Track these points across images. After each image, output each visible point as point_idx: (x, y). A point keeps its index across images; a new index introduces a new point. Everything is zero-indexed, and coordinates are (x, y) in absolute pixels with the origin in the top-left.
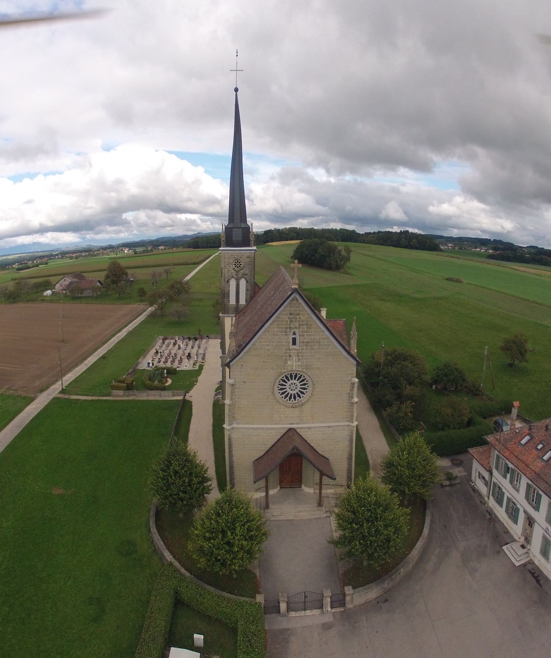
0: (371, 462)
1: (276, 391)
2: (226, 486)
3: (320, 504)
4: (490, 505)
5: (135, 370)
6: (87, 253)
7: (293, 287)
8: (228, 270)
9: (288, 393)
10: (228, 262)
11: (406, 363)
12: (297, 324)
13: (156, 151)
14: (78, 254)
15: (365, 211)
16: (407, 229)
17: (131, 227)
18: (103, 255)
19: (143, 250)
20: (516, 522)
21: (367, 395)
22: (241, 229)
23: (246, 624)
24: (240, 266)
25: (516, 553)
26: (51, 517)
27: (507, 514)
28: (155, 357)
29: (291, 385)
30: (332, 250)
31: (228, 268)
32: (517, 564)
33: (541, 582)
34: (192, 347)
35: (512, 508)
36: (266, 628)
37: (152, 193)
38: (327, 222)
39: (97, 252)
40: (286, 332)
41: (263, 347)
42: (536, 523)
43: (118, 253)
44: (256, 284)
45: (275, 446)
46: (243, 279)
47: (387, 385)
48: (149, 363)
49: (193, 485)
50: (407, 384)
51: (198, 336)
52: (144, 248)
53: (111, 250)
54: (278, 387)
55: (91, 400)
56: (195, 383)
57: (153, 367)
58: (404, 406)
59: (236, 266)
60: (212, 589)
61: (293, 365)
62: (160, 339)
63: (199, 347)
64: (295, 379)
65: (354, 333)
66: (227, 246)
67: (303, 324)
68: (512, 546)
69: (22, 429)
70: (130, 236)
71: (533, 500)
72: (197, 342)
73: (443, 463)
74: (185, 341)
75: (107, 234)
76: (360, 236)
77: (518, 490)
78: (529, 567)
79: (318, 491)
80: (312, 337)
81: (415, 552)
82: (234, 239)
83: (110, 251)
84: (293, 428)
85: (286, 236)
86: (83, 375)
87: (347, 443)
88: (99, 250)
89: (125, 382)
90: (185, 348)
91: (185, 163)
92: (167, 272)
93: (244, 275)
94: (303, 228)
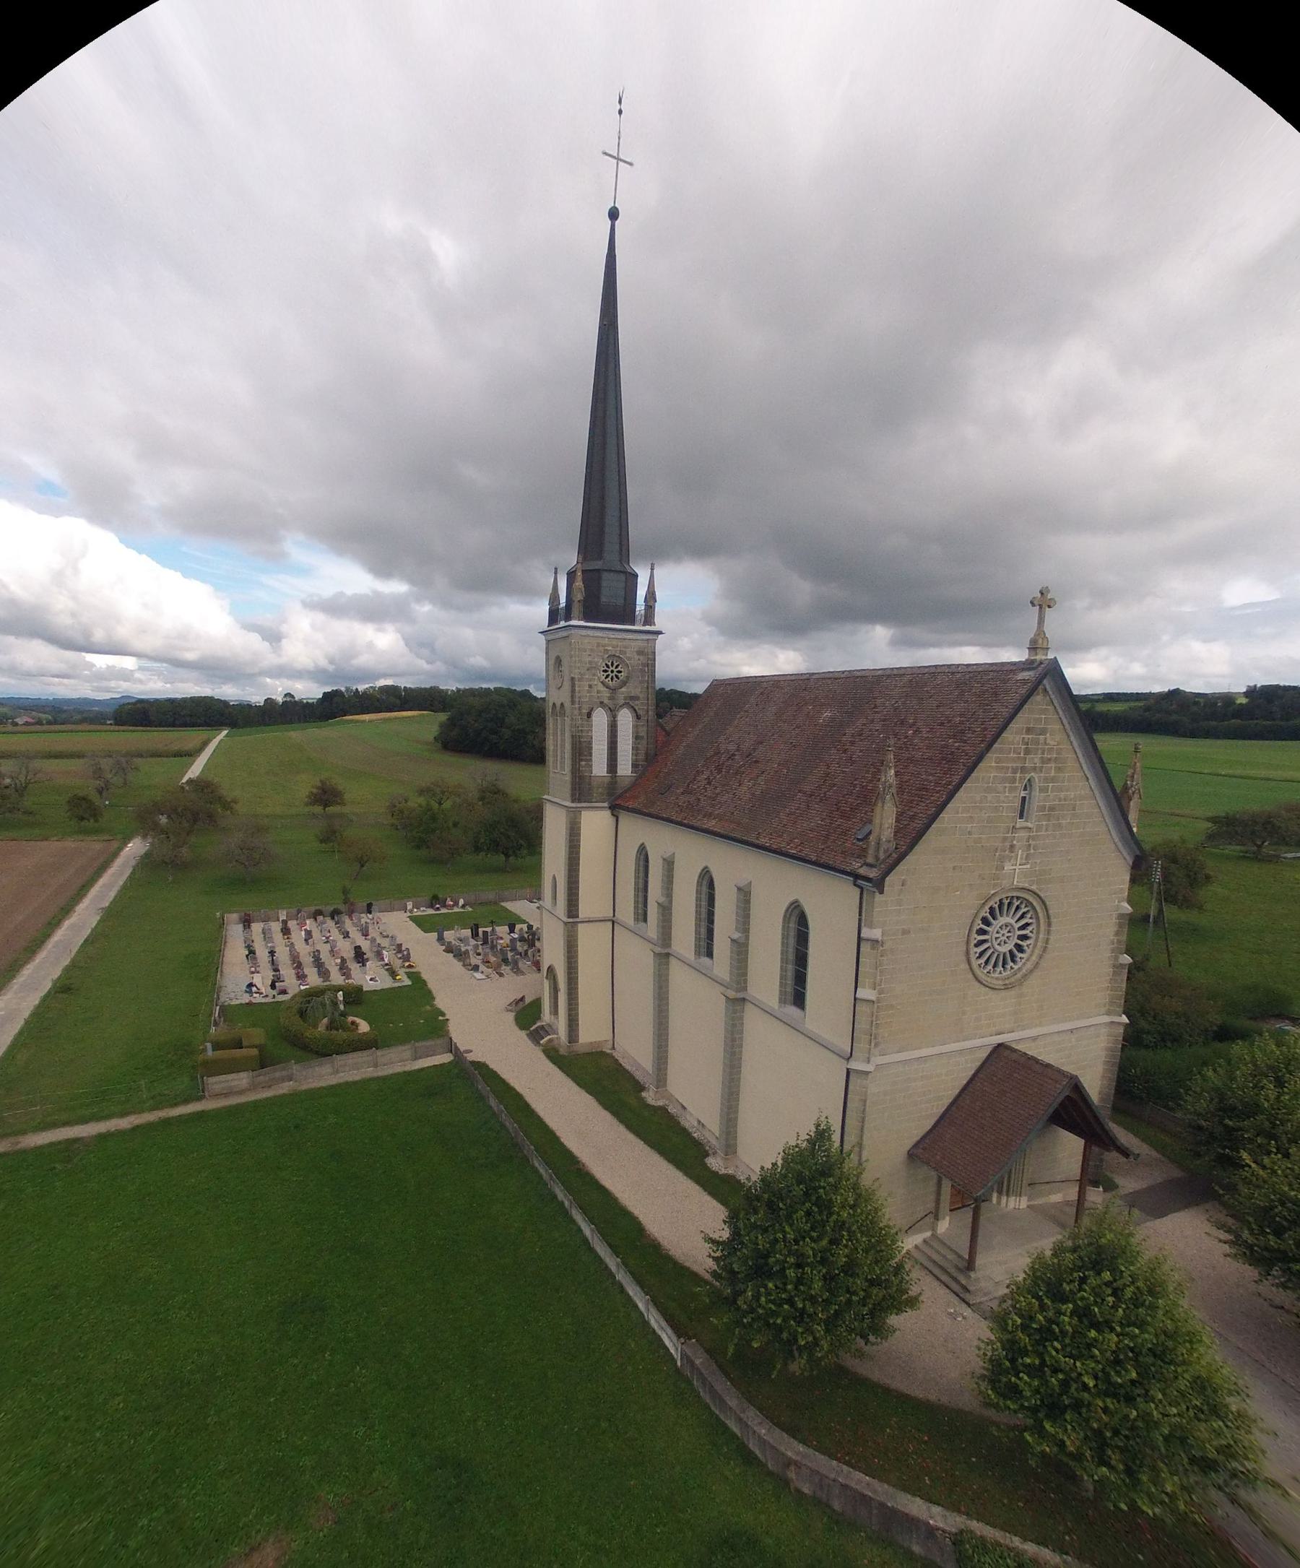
8: (590, 686)
24: (620, 675)
51: (342, 907)
61: (1016, 873)
66: (587, 619)
67: (1050, 759)
80: (1062, 795)
82: (604, 599)
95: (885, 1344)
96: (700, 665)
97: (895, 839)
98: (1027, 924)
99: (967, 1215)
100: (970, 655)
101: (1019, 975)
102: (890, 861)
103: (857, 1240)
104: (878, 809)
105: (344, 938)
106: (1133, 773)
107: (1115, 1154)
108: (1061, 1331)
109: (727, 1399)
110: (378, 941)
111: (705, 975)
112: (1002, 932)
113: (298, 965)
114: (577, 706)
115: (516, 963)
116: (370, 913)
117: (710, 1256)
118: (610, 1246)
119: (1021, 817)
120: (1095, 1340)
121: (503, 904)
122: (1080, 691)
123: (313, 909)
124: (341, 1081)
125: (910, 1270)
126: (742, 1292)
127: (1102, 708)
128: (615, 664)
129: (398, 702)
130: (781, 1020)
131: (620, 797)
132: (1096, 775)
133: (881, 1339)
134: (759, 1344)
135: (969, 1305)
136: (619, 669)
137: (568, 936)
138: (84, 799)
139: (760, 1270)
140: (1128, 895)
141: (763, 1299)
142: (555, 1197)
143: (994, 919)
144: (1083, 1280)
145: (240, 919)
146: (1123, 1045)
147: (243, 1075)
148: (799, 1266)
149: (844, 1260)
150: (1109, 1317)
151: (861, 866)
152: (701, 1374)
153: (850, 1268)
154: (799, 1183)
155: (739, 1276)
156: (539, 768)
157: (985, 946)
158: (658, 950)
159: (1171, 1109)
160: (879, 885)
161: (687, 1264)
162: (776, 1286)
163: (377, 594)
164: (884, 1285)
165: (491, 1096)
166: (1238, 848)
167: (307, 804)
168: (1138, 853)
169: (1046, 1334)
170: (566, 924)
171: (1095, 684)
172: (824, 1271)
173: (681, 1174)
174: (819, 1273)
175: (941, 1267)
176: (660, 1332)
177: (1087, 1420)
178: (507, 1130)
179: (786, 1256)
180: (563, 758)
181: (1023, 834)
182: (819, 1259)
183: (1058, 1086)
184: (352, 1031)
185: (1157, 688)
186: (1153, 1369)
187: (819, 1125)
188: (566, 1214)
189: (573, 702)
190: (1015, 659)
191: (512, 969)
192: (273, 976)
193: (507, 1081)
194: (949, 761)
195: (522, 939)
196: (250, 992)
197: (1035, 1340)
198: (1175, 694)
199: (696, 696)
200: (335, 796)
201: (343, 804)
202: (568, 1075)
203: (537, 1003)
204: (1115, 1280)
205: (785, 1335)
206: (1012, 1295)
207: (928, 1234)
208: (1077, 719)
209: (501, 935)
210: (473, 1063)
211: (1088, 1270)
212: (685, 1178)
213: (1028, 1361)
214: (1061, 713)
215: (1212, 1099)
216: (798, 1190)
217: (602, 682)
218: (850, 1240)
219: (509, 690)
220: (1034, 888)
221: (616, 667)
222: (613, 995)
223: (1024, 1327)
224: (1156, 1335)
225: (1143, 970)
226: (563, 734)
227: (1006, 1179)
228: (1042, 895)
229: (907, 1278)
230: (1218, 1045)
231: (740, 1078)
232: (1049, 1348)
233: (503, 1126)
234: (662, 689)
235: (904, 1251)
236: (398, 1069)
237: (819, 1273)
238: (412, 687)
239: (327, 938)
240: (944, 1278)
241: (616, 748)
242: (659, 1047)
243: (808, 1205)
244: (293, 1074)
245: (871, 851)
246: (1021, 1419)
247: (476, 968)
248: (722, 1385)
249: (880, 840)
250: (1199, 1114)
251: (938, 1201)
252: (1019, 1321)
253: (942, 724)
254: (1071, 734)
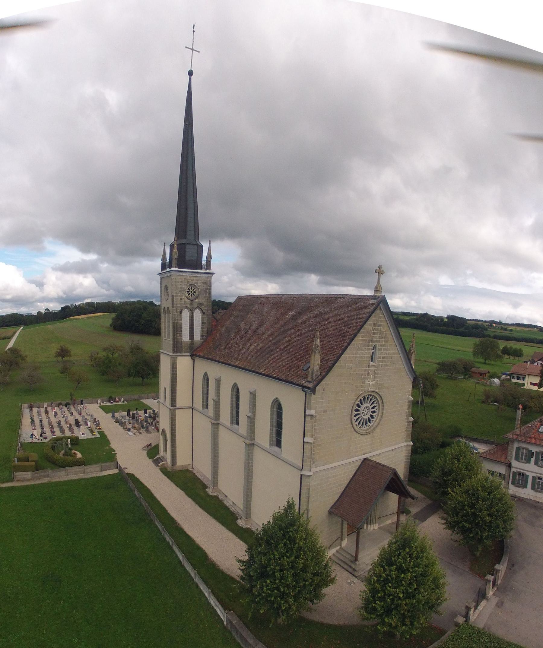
8: (181, 299)
10: (181, 288)
24: (195, 293)
51: (70, 402)
61: (370, 384)
67: (382, 337)
69: (287, 458)
80: (387, 352)
82: (187, 258)
95: (321, 603)
96: (232, 289)
97: (320, 370)
98: (375, 406)
99: (354, 536)
100: (351, 291)
101: (372, 428)
102: (318, 380)
103: (307, 555)
104: (313, 357)
105: (71, 415)
106: (413, 345)
107: (409, 499)
108: (391, 579)
109: (249, 640)
110: (86, 417)
111: (235, 433)
112: (365, 410)
113: (52, 427)
114: (175, 308)
115: (147, 428)
116: (82, 404)
117: (239, 569)
118: (192, 564)
119: (372, 361)
120: (403, 578)
121: (141, 400)
122: (393, 310)
123: (58, 402)
124: (69, 479)
125: (331, 566)
126: (255, 586)
127: (401, 317)
128: (193, 288)
129: (94, 309)
130: (271, 453)
131: (195, 350)
132: (400, 344)
133: (319, 601)
134: (263, 611)
135: (356, 577)
136: (194, 291)
137: (172, 415)
139: (263, 574)
140: (412, 393)
141: (265, 588)
142: (165, 539)
143: (362, 405)
144: (399, 554)
145: (28, 406)
146: (411, 454)
147: (29, 473)
148: (281, 570)
149: (302, 565)
150: (408, 567)
151: (306, 382)
152: (236, 628)
153: (304, 569)
154: (280, 530)
155: (254, 578)
156: (158, 337)
157: (358, 416)
158: (213, 421)
159: (428, 477)
160: (313, 390)
161: (228, 573)
162: (271, 582)
163: (84, 261)
164: (320, 575)
165: (136, 490)
166: (446, 374)
167: (55, 357)
168: (415, 376)
169: (386, 581)
170: (170, 409)
171: (398, 308)
172: (293, 572)
173: (225, 528)
174: (291, 573)
175: (344, 562)
176: (216, 608)
177: (400, 611)
178: (143, 506)
179: (275, 566)
180: (169, 333)
181: (373, 368)
182: (290, 566)
183: (388, 474)
184: (74, 457)
185: (420, 312)
186: (421, 581)
187: (289, 502)
188: (170, 548)
189: (173, 307)
190: (369, 294)
191: (145, 431)
192: (41, 431)
193: (143, 483)
194: (343, 336)
195: (150, 417)
196: (32, 438)
197: (382, 585)
198: (426, 314)
199: (230, 304)
200: (67, 353)
201: (70, 356)
202: (171, 481)
203: (157, 447)
204: (410, 551)
205: (275, 606)
206: (373, 569)
207: (338, 547)
208: (392, 321)
209: (140, 415)
210: (127, 474)
211: (401, 550)
212: (227, 530)
213: (379, 595)
214: (386, 318)
215: (440, 471)
216: (280, 533)
217: (186, 297)
218: (304, 555)
219: (143, 302)
220: (377, 391)
221: (193, 290)
222: (192, 442)
223: (378, 581)
224: (423, 568)
225: (417, 423)
226: (169, 322)
227: (369, 517)
228: (380, 394)
229: (330, 570)
230: (442, 449)
231: (252, 481)
232: (387, 587)
233: (141, 504)
234: (215, 300)
235: (328, 557)
236: (94, 475)
237: (291, 573)
238: (100, 302)
239: (64, 415)
240: (346, 567)
241: (193, 328)
242: (214, 467)
243: (285, 540)
244: (49, 474)
245: (310, 376)
246: (377, 620)
247: (129, 430)
248: (246, 633)
249: (313, 370)
250: (436, 477)
251: (342, 532)
252: (376, 579)
253: (340, 320)
254: (390, 327)
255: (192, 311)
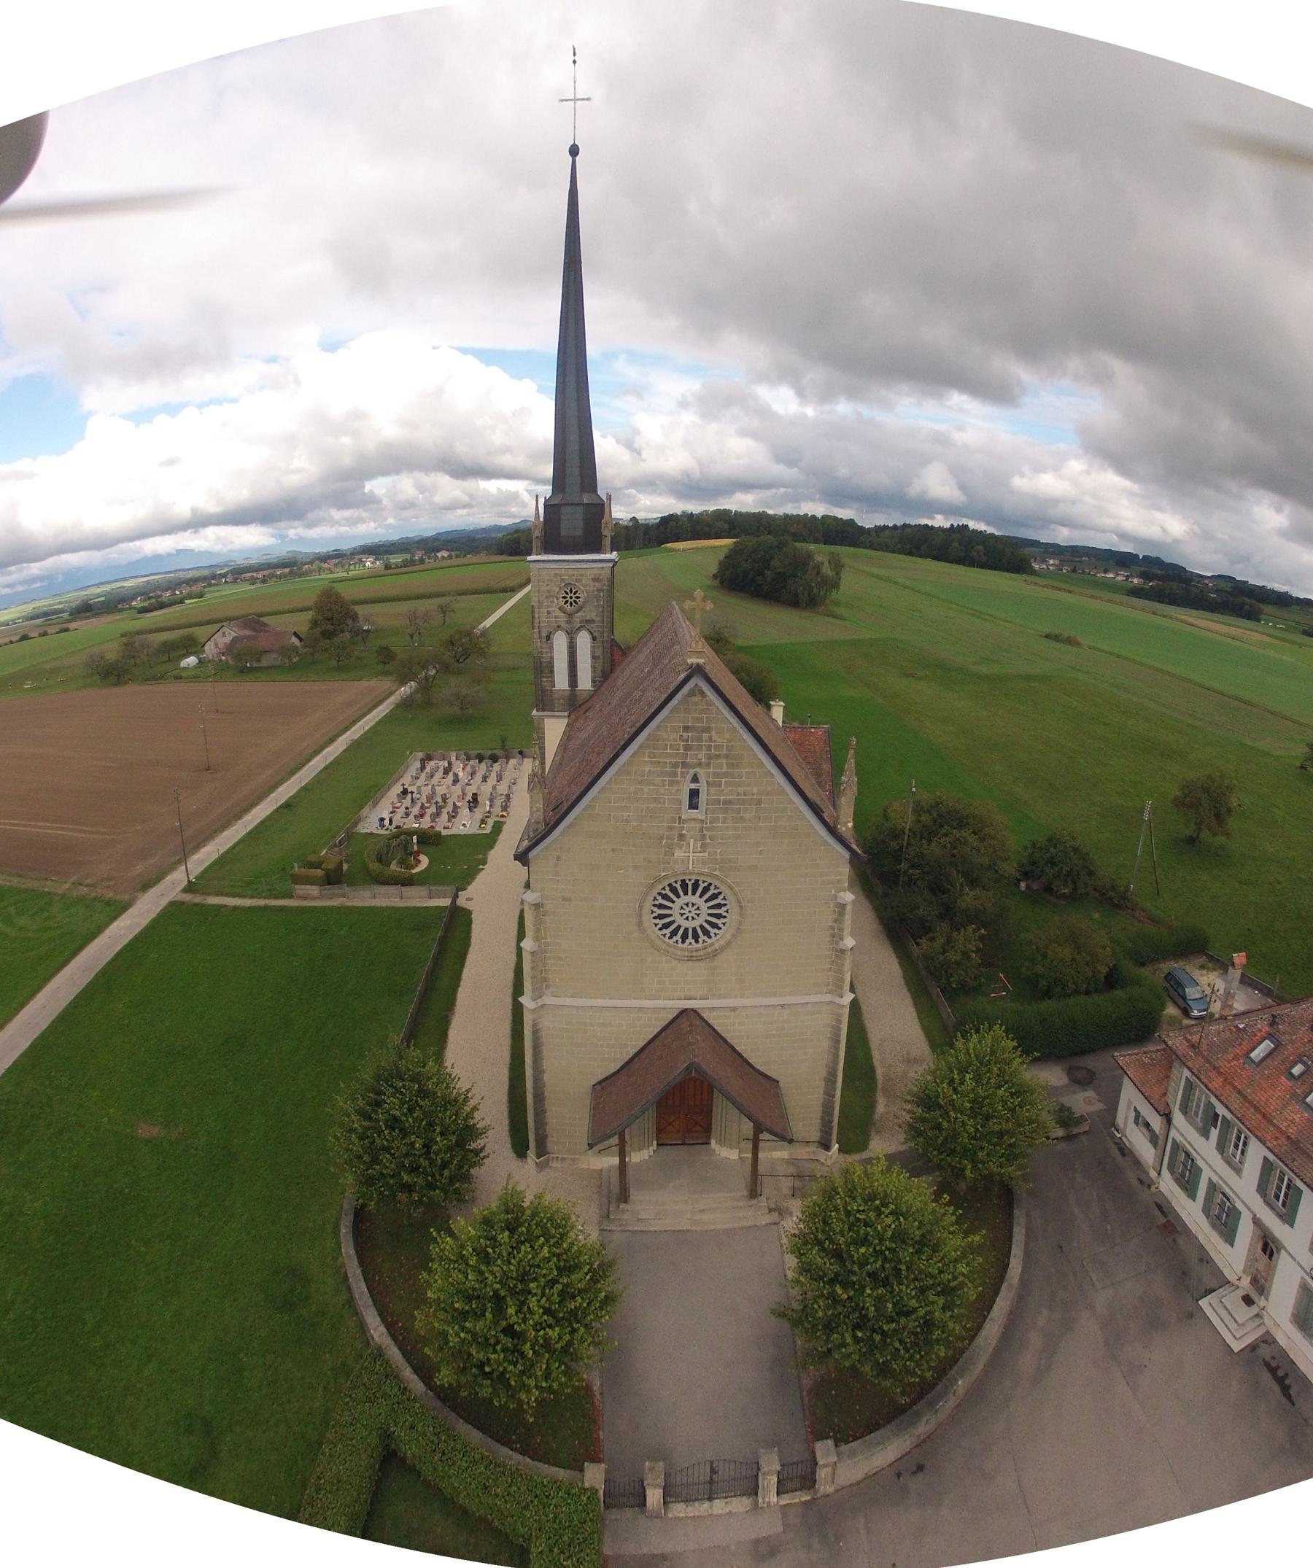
0: (880, 1073)
1: (648, 920)
2: (528, 1148)
3: (754, 1193)
4: (1163, 1187)
5: (350, 836)
6: (287, 570)
7: (689, 661)
9: (679, 927)
10: (548, 591)
11: (963, 833)
12: (702, 756)
13: (434, 348)
14: (267, 573)
15: (877, 478)
16: (964, 521)
17: (383, 509)
18: (319, 571)
19: (403, 561)
20: (1230, 1237)
21: (871, 901)
22: (580, 509)
23: (551, 1551)
25: (1232, 1316)
26: (130, 1193)
27: (1207, 1218)
28: (398, 805)
29: (685, 907)
30: (803, 562)
31: (549, 607)
32: (1237, 1347)
33: (1292, 1392)
34: (485, 779)
35: (1222, 1205)
36: (607, 1550)
37: (428, 436)
38: (795, 500)
39: (307, 566)
40: (675, 774)
41: (612, 814)
42: (1282, 1251)
43: (352, 567)
44: (614, 643)
45: (647, 1051)
46: (583, 631)
47: (919, 883)
48: (382, 820)
49: (437, 1154)
50: (964, 884)
51: (498, 752)
52: (408, 556)
53: (337, 561)
54: (653, 912)
55: (249, 908)
56: (481, 867)
57: (390, 827)
58: (959, 937)
59: (566, 602)
60: (475, 1436)
61: (689, 860)
62: (415, 760)
63: (499, 779)
64: (694, 893)
65: (849, 779)
66: (547, 551)
68: (1223, 1300)
70: (379, 529)
71: (1277, 1197)
72: (497, 767)
73: (1052, 1076)
74: (472, 762)
75: (332, 527)
76: (863, 534)
77: (1238, 1171)
78: (1264, 1351)
79: (750, 1155)
80: (741, 790)
81: (992, 1330)
82: (563, 533)
83: (336, 565)
84: (692, 1009)
85: (707, 529)
86: (237, 849)
87: (825, 1044)
88: (311, 563)
89: (323, 867)
90: (469, 781)
91: (495, 374)
92: (443, 610)
93: (586, 624)
94: (744, 510)
138: (384, 648)
255: (572, 636)
